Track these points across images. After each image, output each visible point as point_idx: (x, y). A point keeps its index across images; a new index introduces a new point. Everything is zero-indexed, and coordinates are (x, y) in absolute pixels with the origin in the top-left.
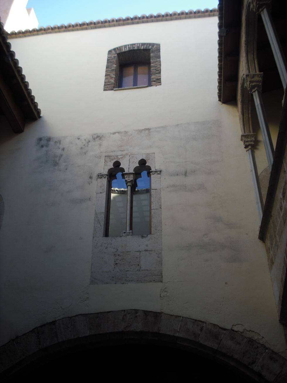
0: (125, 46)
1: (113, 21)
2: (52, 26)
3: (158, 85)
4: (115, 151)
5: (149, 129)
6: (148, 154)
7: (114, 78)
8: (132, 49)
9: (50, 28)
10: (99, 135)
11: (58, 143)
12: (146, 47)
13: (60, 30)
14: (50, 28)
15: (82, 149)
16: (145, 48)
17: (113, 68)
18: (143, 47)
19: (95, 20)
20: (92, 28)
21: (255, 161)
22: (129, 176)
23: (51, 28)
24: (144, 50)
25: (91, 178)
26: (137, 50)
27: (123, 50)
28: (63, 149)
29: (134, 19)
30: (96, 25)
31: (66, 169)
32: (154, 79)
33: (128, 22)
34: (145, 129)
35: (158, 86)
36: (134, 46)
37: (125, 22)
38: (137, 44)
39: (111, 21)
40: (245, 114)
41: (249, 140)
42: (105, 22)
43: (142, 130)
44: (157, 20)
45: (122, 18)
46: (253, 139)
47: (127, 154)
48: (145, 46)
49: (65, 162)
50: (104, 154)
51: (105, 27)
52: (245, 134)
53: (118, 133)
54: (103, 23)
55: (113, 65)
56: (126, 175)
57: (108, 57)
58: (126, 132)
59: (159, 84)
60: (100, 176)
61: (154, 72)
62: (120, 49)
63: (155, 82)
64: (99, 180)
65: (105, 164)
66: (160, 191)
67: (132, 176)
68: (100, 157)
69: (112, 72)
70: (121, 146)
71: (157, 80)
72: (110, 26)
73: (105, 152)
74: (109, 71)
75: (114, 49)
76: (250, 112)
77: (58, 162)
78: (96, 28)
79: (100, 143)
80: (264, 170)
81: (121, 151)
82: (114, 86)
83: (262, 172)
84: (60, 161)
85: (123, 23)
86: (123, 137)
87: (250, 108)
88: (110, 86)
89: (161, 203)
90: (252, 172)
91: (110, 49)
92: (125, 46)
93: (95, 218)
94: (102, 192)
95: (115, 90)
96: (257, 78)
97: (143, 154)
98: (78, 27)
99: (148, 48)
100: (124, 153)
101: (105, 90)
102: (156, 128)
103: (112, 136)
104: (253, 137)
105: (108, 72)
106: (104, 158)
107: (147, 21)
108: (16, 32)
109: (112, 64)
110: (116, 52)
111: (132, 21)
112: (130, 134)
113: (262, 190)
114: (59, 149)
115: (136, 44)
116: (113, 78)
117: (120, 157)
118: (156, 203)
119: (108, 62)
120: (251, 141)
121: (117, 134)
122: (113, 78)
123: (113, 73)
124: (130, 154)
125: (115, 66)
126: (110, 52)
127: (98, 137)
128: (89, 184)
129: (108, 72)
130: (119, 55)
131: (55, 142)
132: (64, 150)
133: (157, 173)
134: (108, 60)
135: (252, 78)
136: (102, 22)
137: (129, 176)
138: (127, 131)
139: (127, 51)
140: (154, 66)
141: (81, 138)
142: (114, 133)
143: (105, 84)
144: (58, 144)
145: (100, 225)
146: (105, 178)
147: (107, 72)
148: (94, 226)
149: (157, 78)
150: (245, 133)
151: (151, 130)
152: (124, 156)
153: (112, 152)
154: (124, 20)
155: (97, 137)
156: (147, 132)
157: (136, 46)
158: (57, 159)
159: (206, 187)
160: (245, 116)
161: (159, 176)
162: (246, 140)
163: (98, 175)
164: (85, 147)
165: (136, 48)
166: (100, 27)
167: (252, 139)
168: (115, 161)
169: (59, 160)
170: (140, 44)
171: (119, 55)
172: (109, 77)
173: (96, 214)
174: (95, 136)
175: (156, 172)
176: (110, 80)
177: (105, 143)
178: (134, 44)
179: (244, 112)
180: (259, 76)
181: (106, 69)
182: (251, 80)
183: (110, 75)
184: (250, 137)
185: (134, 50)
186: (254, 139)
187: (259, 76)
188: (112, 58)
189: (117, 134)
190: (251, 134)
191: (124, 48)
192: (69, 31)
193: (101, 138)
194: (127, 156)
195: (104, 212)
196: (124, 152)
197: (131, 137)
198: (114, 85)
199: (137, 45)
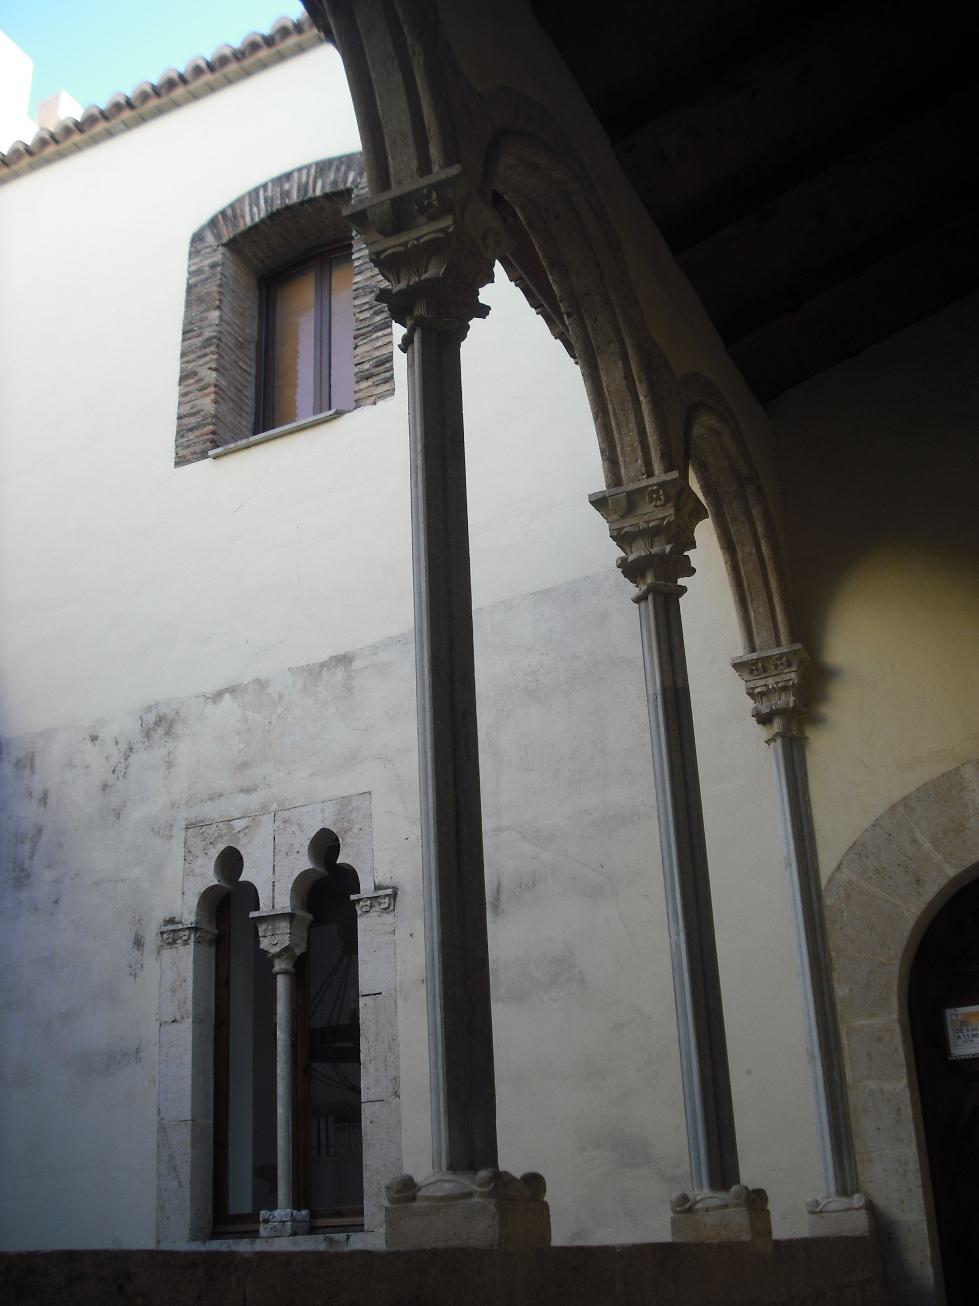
0: (253, 195)
1: (198, 71)
2: (156, 81)
3: (382, 397)
4: (221, 795)
5: (344, 660)
6: (345, 802)
7: (212, 389)
8: (278, 204)
9: (149, 90)
10: (163, 710)
11: (25, 767)
12: (335, 183)
13: (14, 168)
14: (149, 90)
15: (108, 789)
16: (328, 189)
17: (207, 334)
18: (323, 186)
19: (129, 88)
20: (128, 126)
21: (808, 803)
22: (274, 929)
23: (154, 88)
24: (327, 196)
25: (138, 943)
26: (302, 203)
27: (243, 217)
28: (44, 799)
29: (278, 37)
30: (140, 110)
31: (56, 902)
32: (366, 366)
33: (260, 60)
34: (331, 658)
35: (380, 403)
36: (287, 186)
37: (246, 63)
38: (300, 170)
39: (188, 76)
40: (738, 548)
41: (771, 682)
42: (170, 84)
43: (323, 665)
44: (225, 76)
45: (69, 118)
46: (792, 676)
47: (264, 809)
48: (332, 176)
49: (50, 866)
50: (184, 815)
51: (176, 105)
52: (754, 656)
53: (232, 690)
54: (163, 92)
55: (207, 314)
56: (261, 923)
57: (191, 274)
58: (261, 685)
59: (386, 387)
60: (171, 933)
61: (367, 323)
62: (235, 216)
63: (370, 382)
64: (167, 953)
65: (187, 865)
66: (393, 1003)
67: (284, 926)
68: (164, 832)
69: (205, 355)
70: (244, 765)
71: (375, 370)
72: (195, 97)
73: (187, 803)
74: (193, 352)
75: (213, 223)
76: (760, 530)
77: (27, 864)
78: (143, 120)
79: (169, 753)
80: (847, 853)
81: (242, 791)
82: (213, 433)
83: (839, 868)
84: (35, 858)
85: (243, 69)
86: (249, 713)
87: (756, 511)
88: (197, 433)
89: (397, 1068)
90: (788, 871)
91: (194, 227)
92: (254, 194)
93: (158, 1147)
94: (178, 1018)
95: (215, 458)
96: (650, 508)
97: (323, 802)
98: (233, 67)
99: (341, 187)
100: (254, 801)
101: (181, 461)
102: (374, 649)
103: (211, 708)
104: (789, 666)
105: (192, 357)
106: (183, 834)
107: (243, 69)
108: (29, 143)
109: (206, 310)
110: (218, 236)
111: (273, 50)
112: (277, 697)
113: (835, 975)
114: (31, 795)
115: (296, 175)
116: (209, 386)
117: (239, 825)
118: (377, 1069)
119: (189, 304)
120: (784, 689)
121: (227, 696)
122: (209, 386)
123: (207, 359)
124: (275, 806)
125: (215, 315)
126: (197, 238)
127: (161, 724)
128: (132, 978)
129: (192, 357)
130: (233, 245)
131: (16, 764)
132: (45, 804)
133: (380, 904)
134: (190, 288)
135: (623, 516)
136: (157, 91)
137: (274, 929)
138: (264, 679)
139: (262, 221)
140: (363, 288)
141: (101, 736)
142: (219, 695)
143: (179, 426)
144: (27, 772)
145: (176, 1184)
146: (186, 943)
147: (186, 359)
148: (159, 1187)
149: (377, 353)
150: (753, 649)
151: (356, 665)
152: (253, 818)
153: (211, 799)
154: (239, 56)
155: (155, 724)
156: (339, 673)
157: (296, 186)
158: (26, 849)
159: (581, 972)
160: (740, 555)
161: (388, 918)
162: (759, 685)
163: (162, 933)
164: (118, 778)
165: (294, 198)
166: (159, 112)
167: (787, 677)
168: (221, 847)
169: (32, 856)
170: (308, 167)
171: (233, 245)
172: (195, 387)
173: (162, 1128)
174: (151, 718)
175: (376, 904)
176: (198, 402)
177: (185, 750)
178: (288, 176)
179: (735, 538)
180: (659, 498)
181: (184, 340)
182: (621, 529)
183: (196, 374)
184: (776, 667)
185: (288, 208)
186: (793, 675)
187: (659, 498)
188: (202, 277)
189: (227, 696)
190: (784, 649)
191: (247, 209)
192: (49, 161)
193: (171, 726)
194: (267, 816)
195: (187, 1114)
196: (255, 795)
197: (279, 709)
198: (211, 427)
199: (300, 178)
